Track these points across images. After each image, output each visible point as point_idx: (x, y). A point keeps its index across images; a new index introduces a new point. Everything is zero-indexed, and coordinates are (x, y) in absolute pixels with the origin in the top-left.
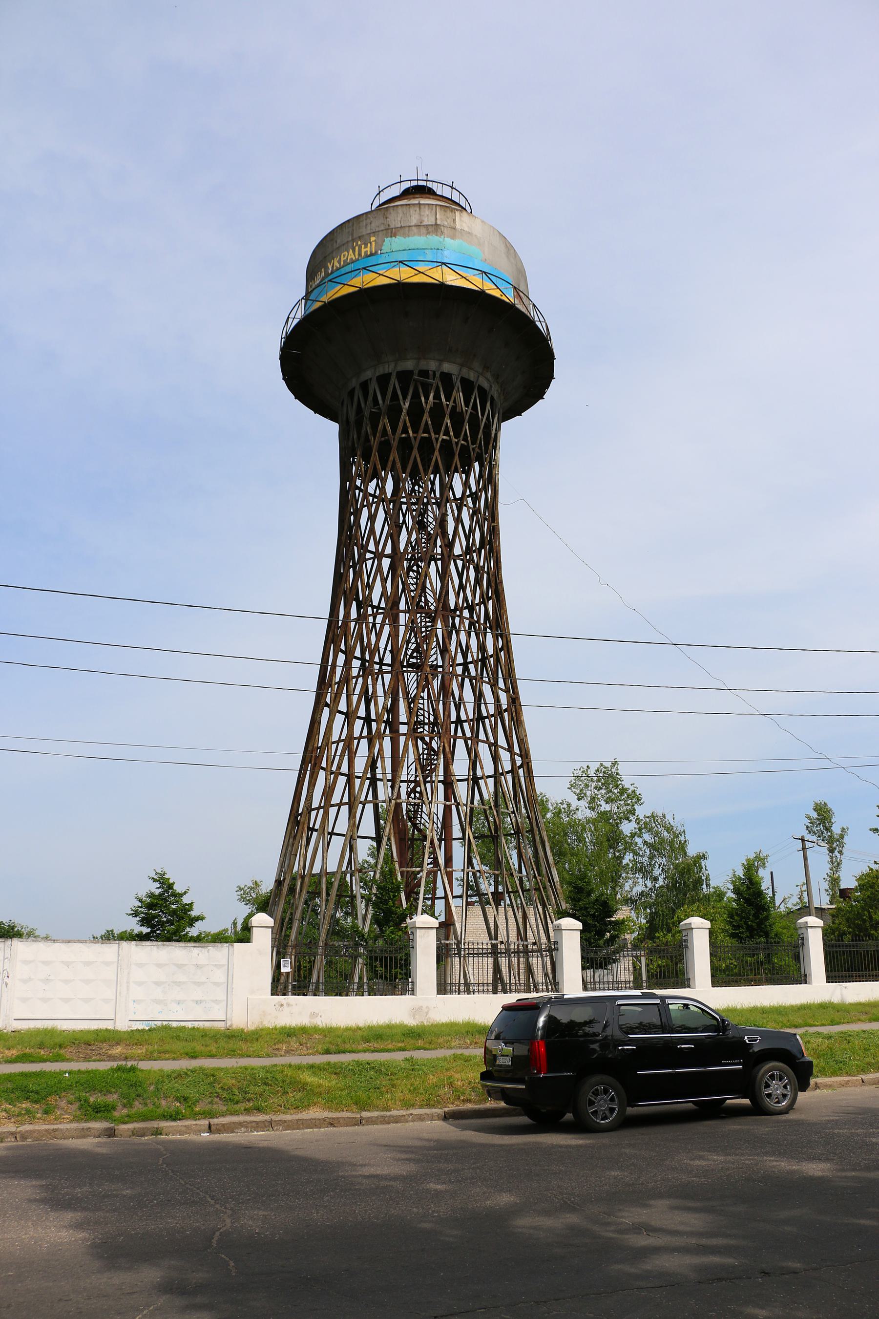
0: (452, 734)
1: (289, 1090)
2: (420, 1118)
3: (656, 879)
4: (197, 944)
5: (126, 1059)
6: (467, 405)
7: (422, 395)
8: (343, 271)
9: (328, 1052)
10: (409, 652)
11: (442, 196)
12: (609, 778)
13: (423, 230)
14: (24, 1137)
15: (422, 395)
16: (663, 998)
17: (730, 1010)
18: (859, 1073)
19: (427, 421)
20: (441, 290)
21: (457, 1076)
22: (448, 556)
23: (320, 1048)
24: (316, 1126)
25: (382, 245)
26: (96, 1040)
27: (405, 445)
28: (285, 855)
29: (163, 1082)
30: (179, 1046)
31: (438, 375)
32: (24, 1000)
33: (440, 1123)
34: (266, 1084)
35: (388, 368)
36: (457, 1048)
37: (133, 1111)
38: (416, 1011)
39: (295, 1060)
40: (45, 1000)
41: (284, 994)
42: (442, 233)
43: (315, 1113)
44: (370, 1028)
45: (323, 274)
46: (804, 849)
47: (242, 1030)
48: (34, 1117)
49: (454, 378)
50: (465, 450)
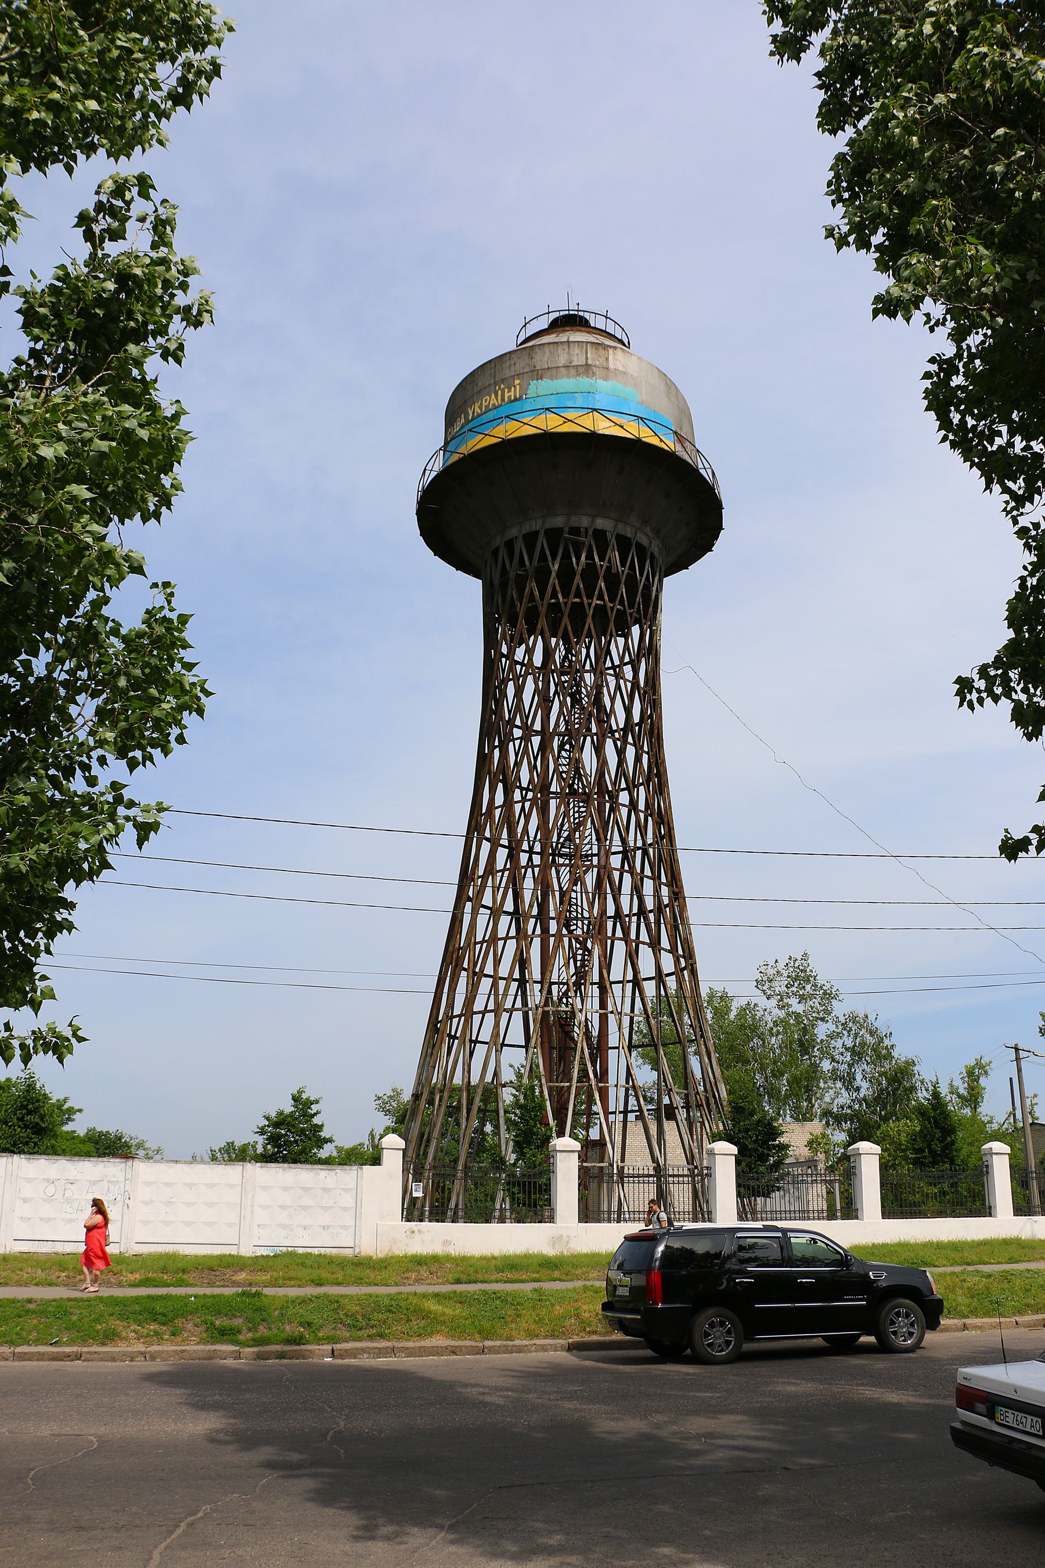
0: (609, 934)
1: (413, 1318)
2: (544, 1348)
3: (858, 1089)
4: (324, 1167)
5: (250, 1285)
6: (623, 565)
7: (573, 555)
8: (485, 418)
9: (458, 1282)
10: (562, 840)
11: (595, 328)
12: (801, 977)
13: (573, 371)
14: (153, 1358)
15: (573, 555)
16: (784, 1231)
17: (857, 1248)
18: (1014, 1314)
19: (578, 585)
20: (592, 440)
21: (585, 1307)
22: (605, 732)
23: (450, 1277)
24: (438, 1354)
25: (527, 389)
26: (219, 1265)
27: (555, 609)
28: (423, 1065)
29: (287, 1307)
30: (304, 1273)
31: (590, 532)
32: (146, 1223)
33: (565, 1353)
34: (390, 1311)
35: (535, 525)
36: (595, 1279)
37: (258, 1335)
38: (555, 1240)
39: (420, 1289)
40: (168, 1223)
41: (421, 1221)
42: (594, 374)
43: (438, 1341)
44: (505, 1258)
45: (463, 420)
46: (1018, 1059)
47: (371, 1258)
48: (162, 1339)
49: (609, 535)
50: (621, 615)
